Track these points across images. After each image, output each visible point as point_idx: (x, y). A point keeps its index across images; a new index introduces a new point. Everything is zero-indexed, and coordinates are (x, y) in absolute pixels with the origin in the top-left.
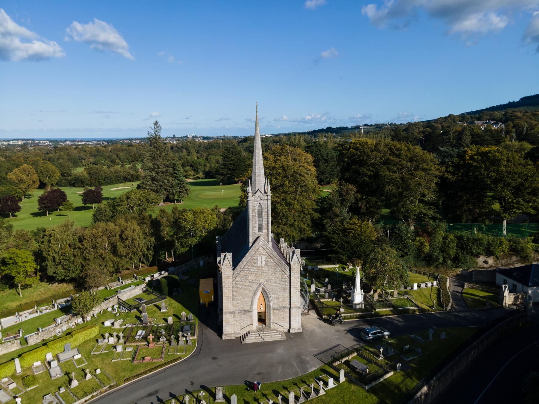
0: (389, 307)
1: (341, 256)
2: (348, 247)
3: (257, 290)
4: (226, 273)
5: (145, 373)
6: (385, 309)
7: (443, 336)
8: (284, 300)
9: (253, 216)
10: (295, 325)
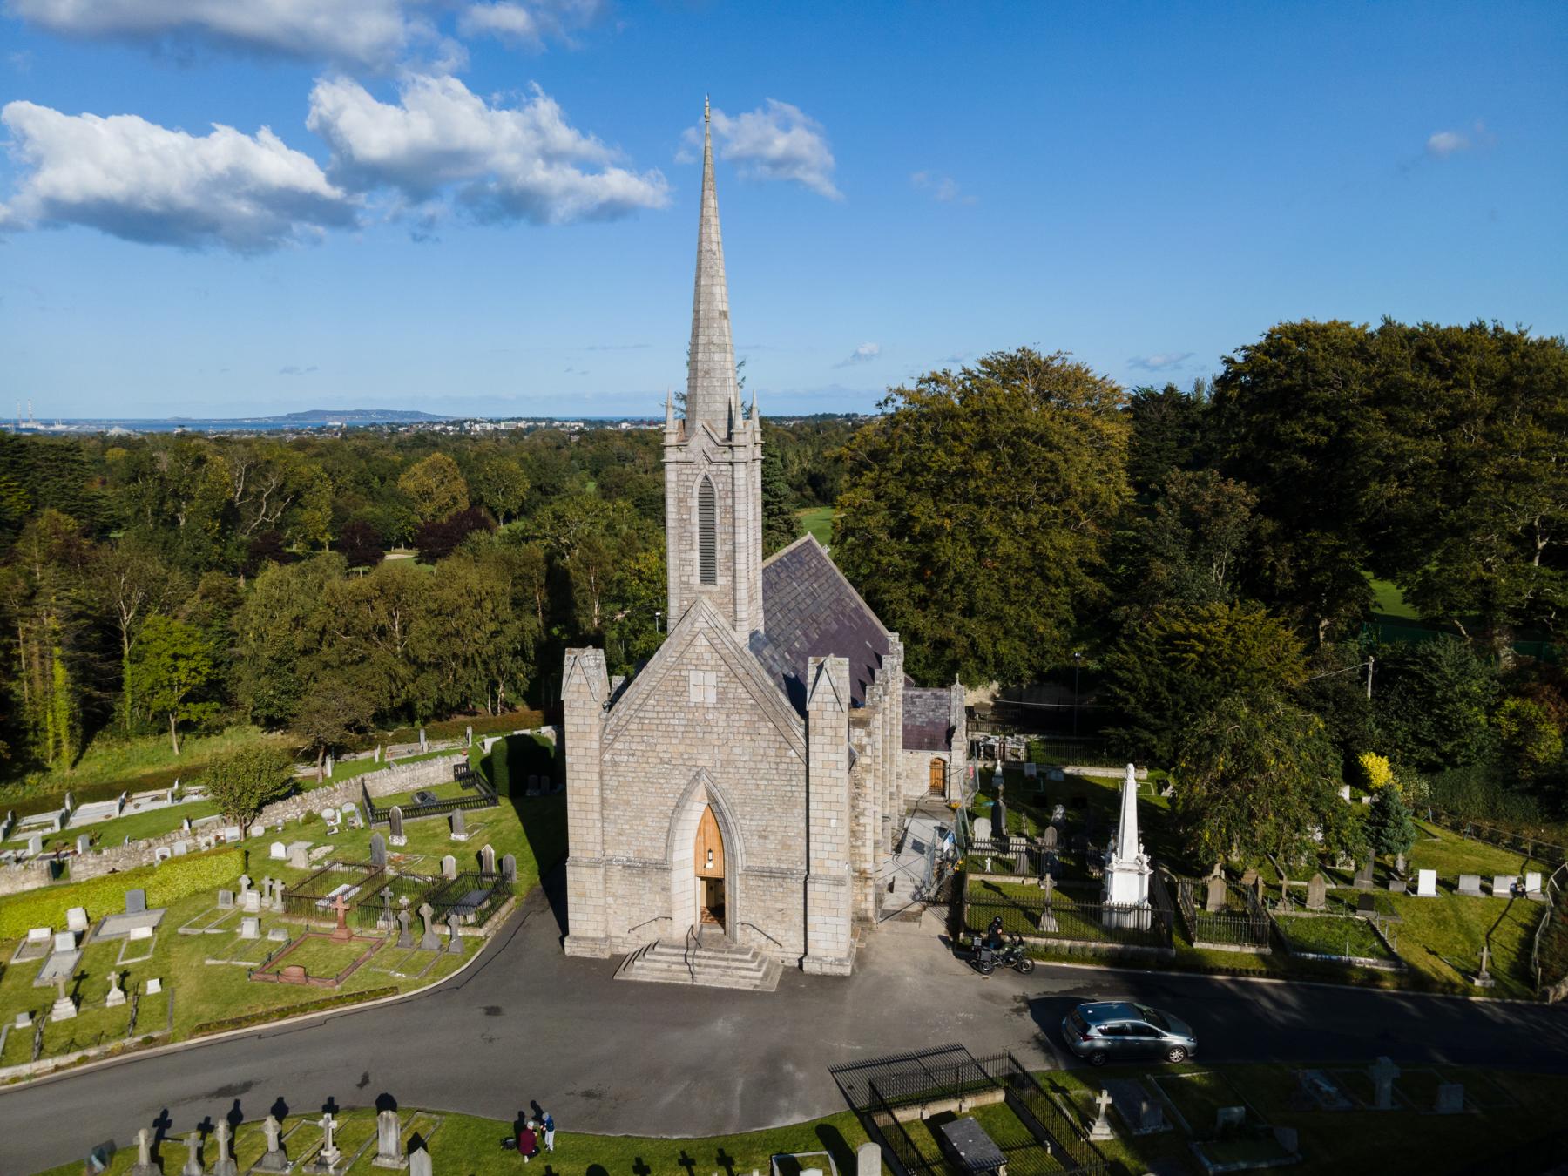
0: (1256, 941)
1: (1146, 735)
2: (1176, 704)
3: (686, 794)
4: (576, 720)
5: (266, 1017)
6: (1234, 949)
7: (1451, 1100)
8: (785, 846)
9: (680, 520)
10: (822, 945)
